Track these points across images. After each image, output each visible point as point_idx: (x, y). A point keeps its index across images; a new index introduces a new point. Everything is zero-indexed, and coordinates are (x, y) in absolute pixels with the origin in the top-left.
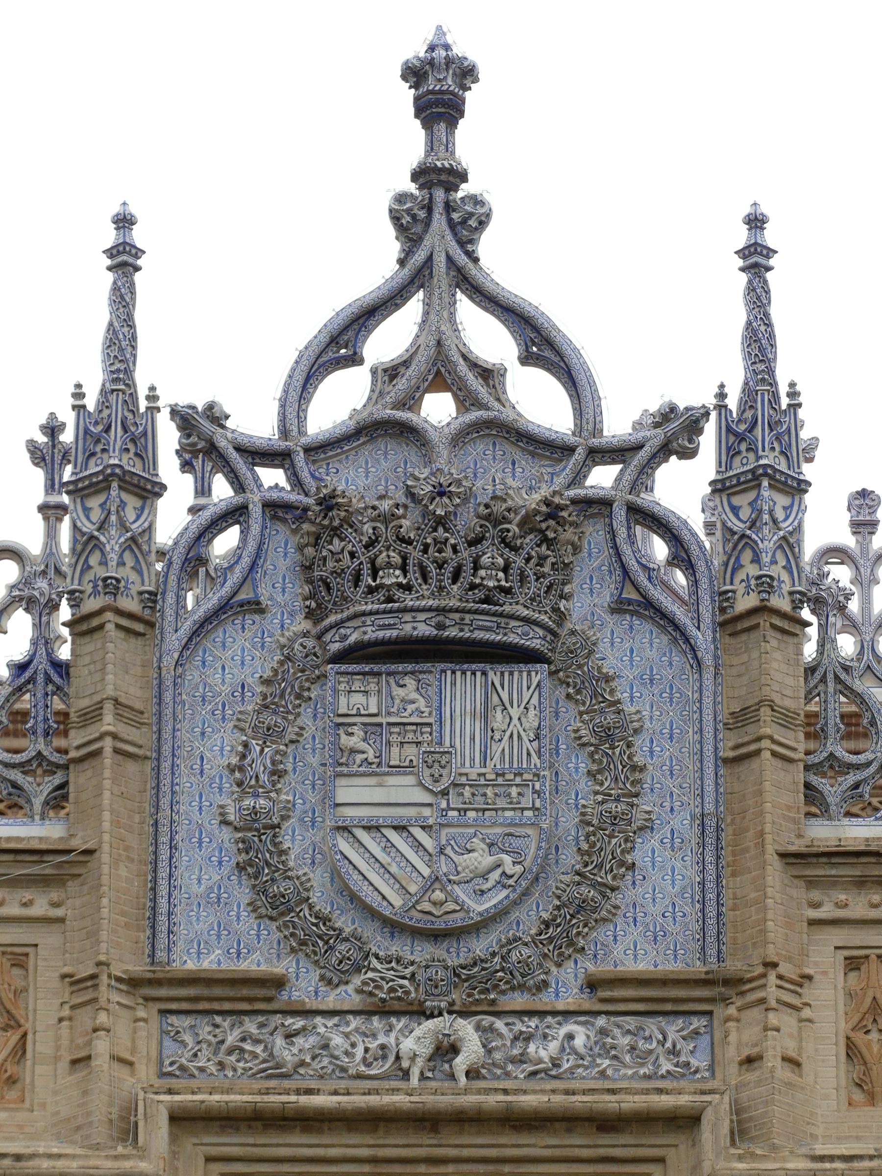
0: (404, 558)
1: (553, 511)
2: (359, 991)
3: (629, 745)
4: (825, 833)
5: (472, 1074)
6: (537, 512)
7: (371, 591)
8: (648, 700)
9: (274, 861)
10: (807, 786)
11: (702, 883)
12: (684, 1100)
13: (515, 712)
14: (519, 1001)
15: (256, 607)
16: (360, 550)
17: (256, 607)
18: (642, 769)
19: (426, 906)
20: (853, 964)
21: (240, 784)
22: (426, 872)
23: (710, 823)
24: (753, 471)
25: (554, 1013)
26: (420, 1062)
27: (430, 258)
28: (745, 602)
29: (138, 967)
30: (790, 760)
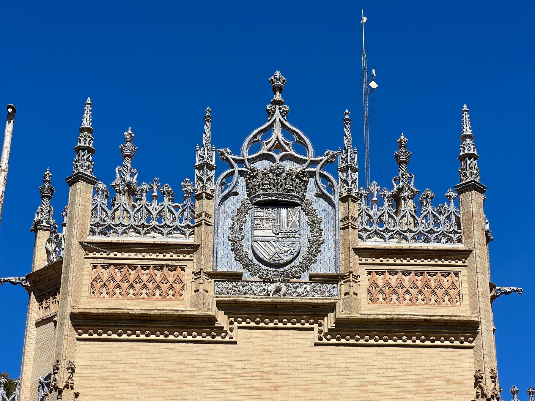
0: (270, 182)
1: (303, 173)
2: (259, 277)
3: (319, 224)
4: (362, 244)
5: (284, 295)
6: (299, 173)
7: (262, 189)
8: (323, 215)
9: (240, 248)
10: (359, 234)
11: (336, 255)
12: (332, 301)
13: (294, 217)
14: (295, 280)
15: (236, 194)
16: (260, 180)
17: (236, 194)
18: (322, 230)
19: (274, 258)
20: (369, 273)
21: (232, 231)
22: (274, 251)
23: (337, 242)
24: (347, 166)
25: (302, 283)
26: (272, 292)
27: (275, 119)
28: (344, 194)
29: (210, 270)
30: (355, 229)
